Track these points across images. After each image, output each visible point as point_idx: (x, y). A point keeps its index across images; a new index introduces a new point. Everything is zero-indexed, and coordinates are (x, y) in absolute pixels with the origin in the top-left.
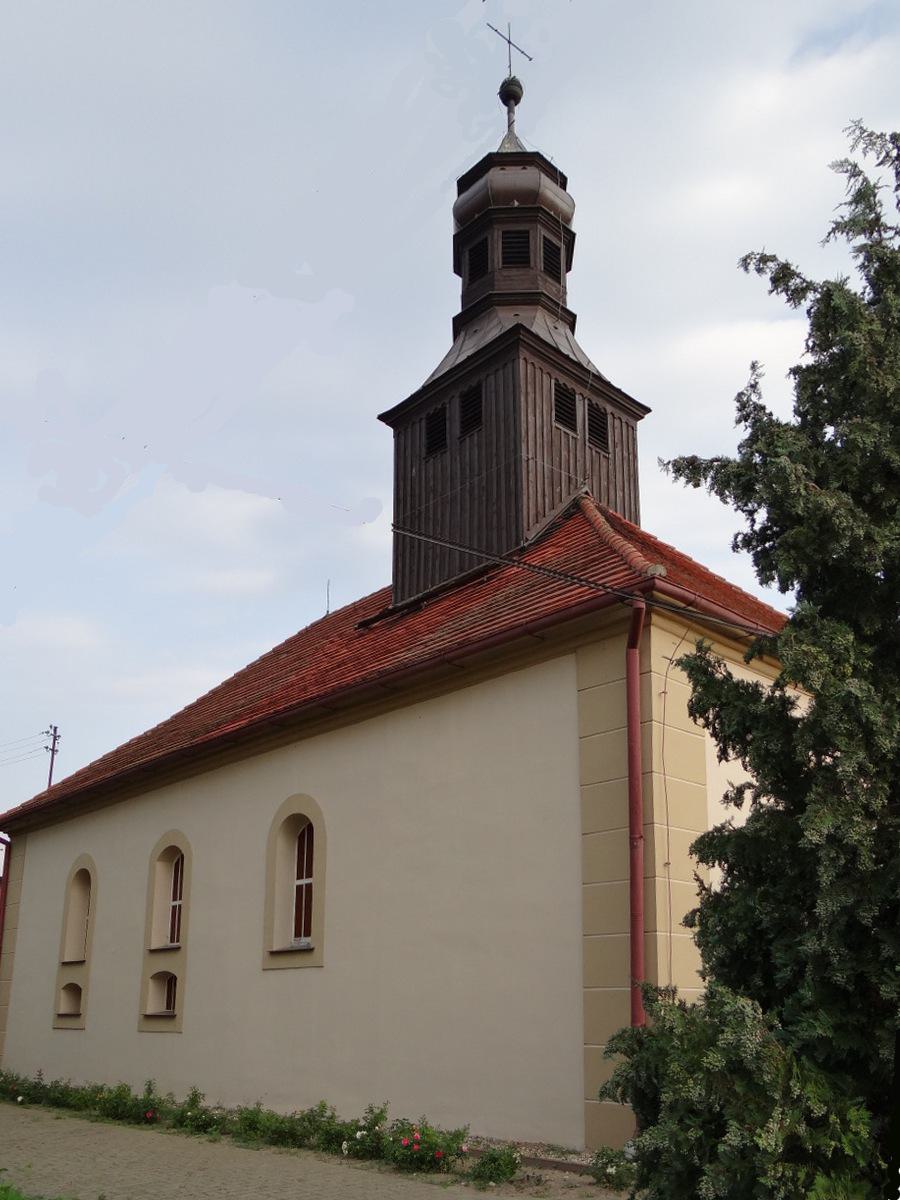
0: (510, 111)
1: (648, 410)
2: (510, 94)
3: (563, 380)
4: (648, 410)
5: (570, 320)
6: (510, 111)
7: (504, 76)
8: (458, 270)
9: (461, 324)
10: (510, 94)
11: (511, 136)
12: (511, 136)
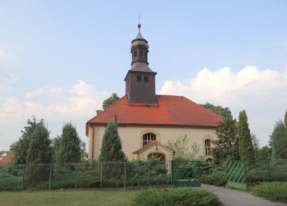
0: (139, 29)
1: (156, 73)
2: (139, 26)
3: (145, 75)
4: (156, 73)
5: (148, 64)
6: (139, 28)
10: (139, 26)
11: (140, 34)
12: (140, 34)
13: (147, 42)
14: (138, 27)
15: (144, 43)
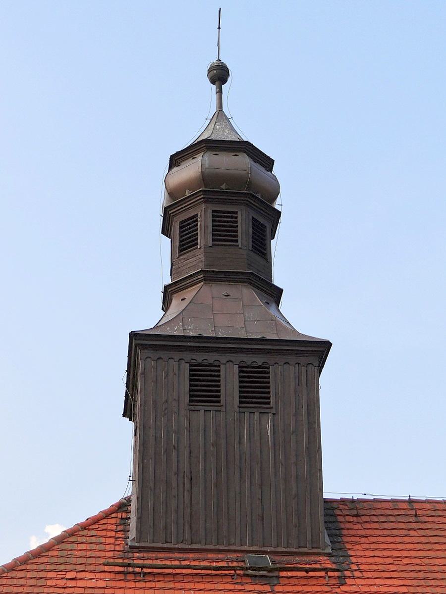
0: (220, 92)
5: (275, 294)
6: (220, 92)
7: (214, 60)
8: (166, 230)
9: (169, 293)
13: (267, 163)
14: (213, 82)
15: (243, 161)
